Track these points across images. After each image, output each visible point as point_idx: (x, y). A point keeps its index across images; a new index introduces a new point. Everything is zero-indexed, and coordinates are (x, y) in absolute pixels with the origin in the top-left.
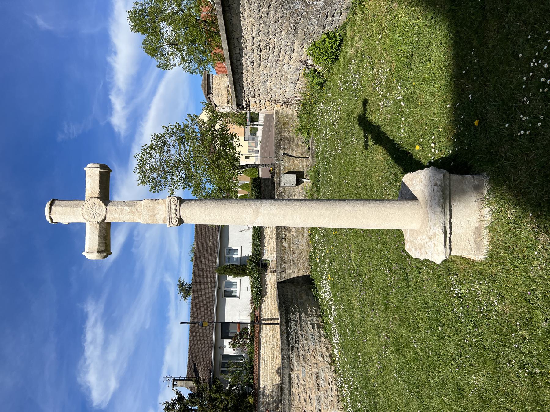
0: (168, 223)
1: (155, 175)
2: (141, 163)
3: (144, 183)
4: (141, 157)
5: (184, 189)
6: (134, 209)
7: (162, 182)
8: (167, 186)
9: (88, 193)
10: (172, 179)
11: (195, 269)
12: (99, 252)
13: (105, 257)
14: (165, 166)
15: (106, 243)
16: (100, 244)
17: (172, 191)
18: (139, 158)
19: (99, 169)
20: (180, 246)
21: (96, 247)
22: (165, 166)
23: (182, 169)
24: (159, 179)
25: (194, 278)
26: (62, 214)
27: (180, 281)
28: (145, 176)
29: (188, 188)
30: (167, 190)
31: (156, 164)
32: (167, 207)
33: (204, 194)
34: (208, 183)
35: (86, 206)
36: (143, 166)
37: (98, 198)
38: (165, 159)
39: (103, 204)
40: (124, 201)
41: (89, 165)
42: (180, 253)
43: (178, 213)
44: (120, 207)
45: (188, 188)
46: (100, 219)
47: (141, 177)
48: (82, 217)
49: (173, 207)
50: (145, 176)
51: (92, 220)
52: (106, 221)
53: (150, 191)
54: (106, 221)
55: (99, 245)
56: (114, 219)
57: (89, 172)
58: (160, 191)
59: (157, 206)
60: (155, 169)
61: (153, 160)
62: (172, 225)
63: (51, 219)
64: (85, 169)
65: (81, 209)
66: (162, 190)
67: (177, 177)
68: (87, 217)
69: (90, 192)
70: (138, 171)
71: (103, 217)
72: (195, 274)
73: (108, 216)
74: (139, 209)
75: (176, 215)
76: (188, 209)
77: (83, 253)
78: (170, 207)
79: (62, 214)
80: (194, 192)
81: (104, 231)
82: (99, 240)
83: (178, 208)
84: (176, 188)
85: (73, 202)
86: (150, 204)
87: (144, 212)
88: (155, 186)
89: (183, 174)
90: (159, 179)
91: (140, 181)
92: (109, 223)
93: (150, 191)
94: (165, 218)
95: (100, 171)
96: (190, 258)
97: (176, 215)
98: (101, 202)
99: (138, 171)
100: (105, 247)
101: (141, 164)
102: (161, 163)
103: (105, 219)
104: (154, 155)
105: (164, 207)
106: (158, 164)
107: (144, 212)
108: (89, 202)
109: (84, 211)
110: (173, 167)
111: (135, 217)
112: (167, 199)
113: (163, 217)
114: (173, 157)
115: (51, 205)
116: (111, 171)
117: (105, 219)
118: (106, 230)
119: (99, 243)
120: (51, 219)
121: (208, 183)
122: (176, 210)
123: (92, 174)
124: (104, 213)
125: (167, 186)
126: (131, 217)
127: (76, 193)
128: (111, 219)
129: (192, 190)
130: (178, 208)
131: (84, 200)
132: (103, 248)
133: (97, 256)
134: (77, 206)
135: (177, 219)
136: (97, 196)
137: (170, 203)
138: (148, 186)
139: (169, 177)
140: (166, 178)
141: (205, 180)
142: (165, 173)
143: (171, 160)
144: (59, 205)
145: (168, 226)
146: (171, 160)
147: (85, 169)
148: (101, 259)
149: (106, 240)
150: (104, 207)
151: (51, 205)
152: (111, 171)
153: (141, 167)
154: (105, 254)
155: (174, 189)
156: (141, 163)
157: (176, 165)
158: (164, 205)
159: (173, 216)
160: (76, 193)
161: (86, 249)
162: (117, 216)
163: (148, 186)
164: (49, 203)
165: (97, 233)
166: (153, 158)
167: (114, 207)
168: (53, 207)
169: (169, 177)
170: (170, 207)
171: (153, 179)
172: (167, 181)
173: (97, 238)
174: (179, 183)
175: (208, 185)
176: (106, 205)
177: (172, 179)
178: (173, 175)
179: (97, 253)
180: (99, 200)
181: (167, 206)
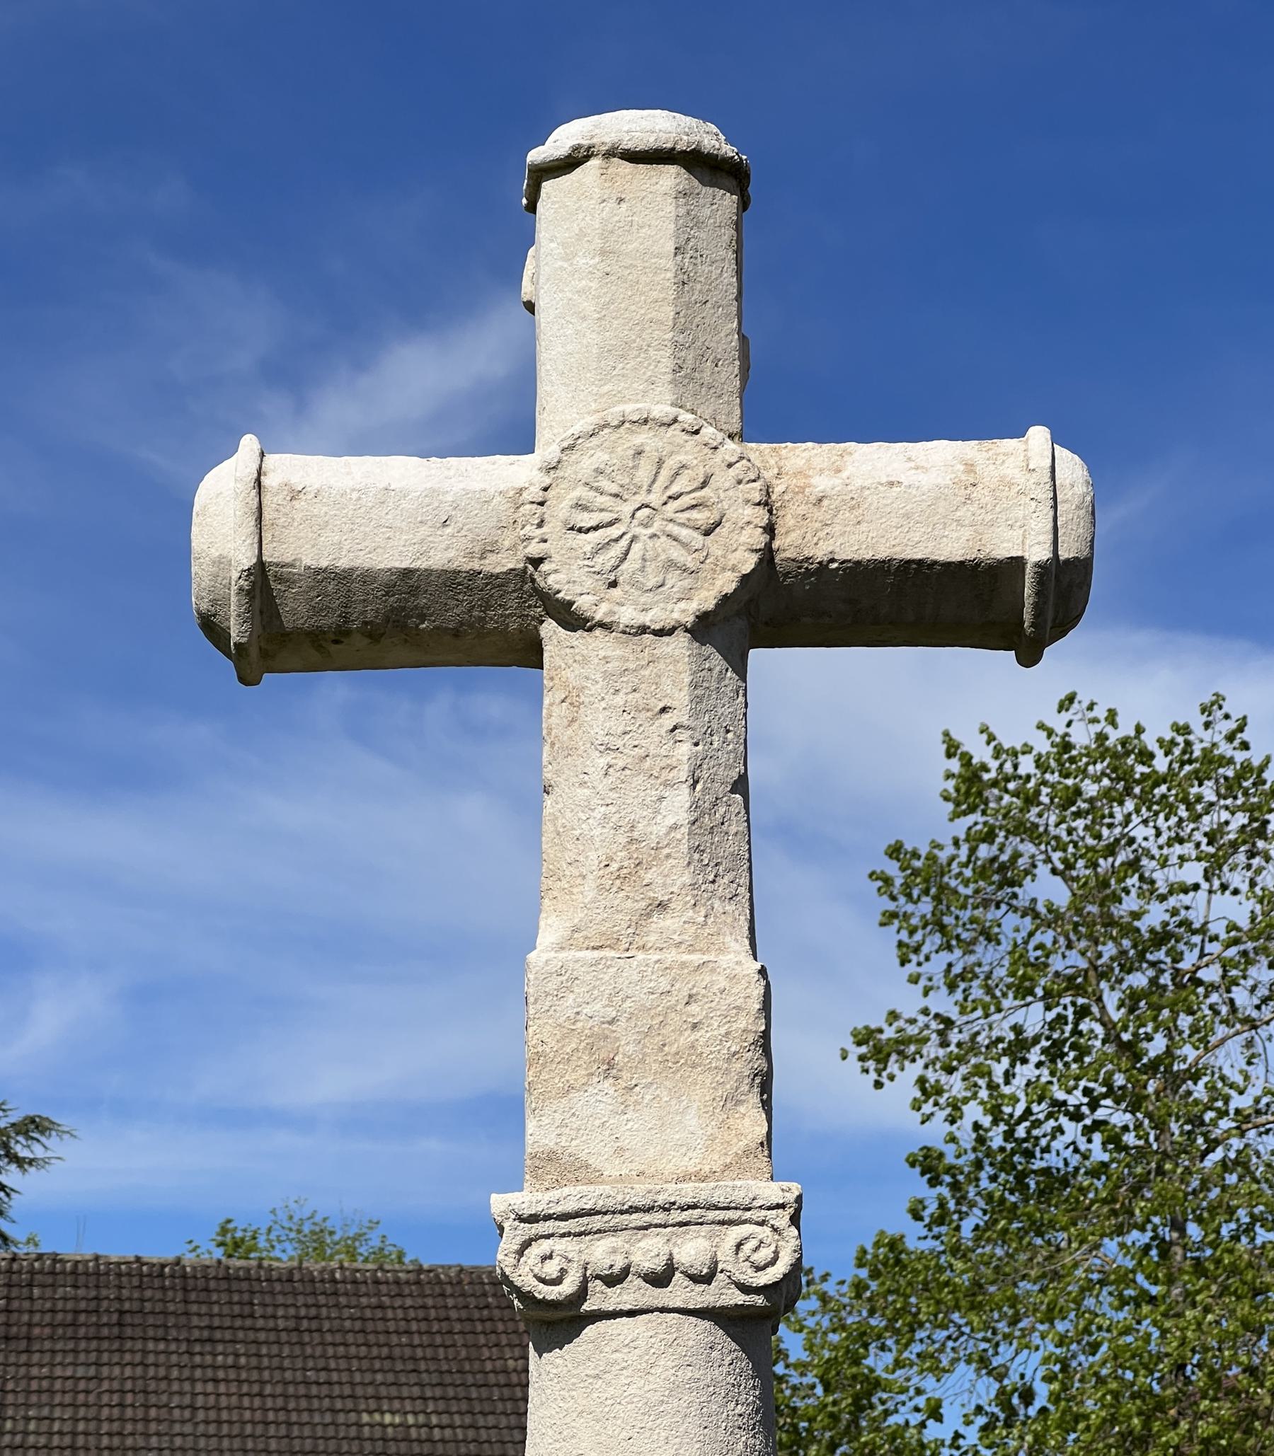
0: (528, 1199)
1: (1048, 889)
2: (1161, 764)
3: (970, 787)
4: (1211, 760)
5: (928, 1164)
6: (673, 876)
7: (986, 954)
8: (944, 1003)
9: (809, 466)
10: (1018, 1048)
11: (145, 1276)
12: (262, 582)
13: (212, 628)
14: (1139, 980)
15: (341, 634)
16: (339, 582)
17: (903, 1048)
18: (1201, 739)
19: (1037, 552)
20: (360, 1120)
21: (306, 547)
22: (1139, 980)
23: (1114, 1140)
24: (1012, 926)
25: (53, 1271)
26: (612, 247)
27: (34, 1126)
28: (1031, 800)
29: (930, 1196)
30: (910, 1002)
31: (1149, 888)
32: (688, 1192)
33: (878, 1362)
34: (987, 1390)
35: (689, 451)
36: (1125, 776)
37: (767, 555)
38: (1211, 974)
39: (706, 599)
40: (740, 785)
41: (1072, 469)
42: (303, 1122)
43: (631, 1294)
44: (685, 749)
45: (930, 1196)
46: (563, 578)
47: (1027, 765)
48: (585, 423)
49: (691, 1250)
50: (1031, 800)
51: (560, 509)
52: (549, 629)
53: (895, 851)
54: (549, 629)
55: (321, 576)
56: (572, 700)
57: (1012, 469)
58: (893, 934)
59: (703, 1088)
60: (1103, 891)
61: (1193, 872)
62: (509, 1243)
63: (569, 164)
64: (1039, 436)
65: (662, 410)
66: (906, 953)
67: (1038, 1092)
68: (586, 462)
69: (821, 483)
70: (1082, 737)
71: (583, 604)
72: (93, 1275)
73: (597, 643)
74: (667, 923)
75: (613, 1280)
76: (674, 1389)
77: (249, 443)
78: (686, 1216)
79: (612, 247)
80: (889, 1258)
81: (455, 614)
82: (368, 577)
83: (680, 1293)
84: (928, 1090)
85: (725, 339)
86: (716, 1029)
87: (638, 975)
88: (943, 895)
89: (1065, 1145)
90: (1012, 926)
91: (981, 753)
92: (531, 654)
93: (895, 851)
94: (579, 1171)
95: (1017, 563)
96: (250, 1212)
97: (613, 1280)
98: (727, 583)
99: (1082, 737)
100: (306, 630)
101: (1146, 757)
102: (1161, 937)
103: (573, 620)
104: (1238, 879)
105: (690, 1163)
106: (1155, 916)
107: (638, 975)
108: (724, 479)
109: (643, 437)
110: (1131, 1050)
111: (589, 890)
112: (773, 1192)
113: (595, 1150)
114: (1229, 1059)
115: (697, 163)
116: (1029, 657)
117: (573, 620)
118: (475, 627)
119: (344, 578)
120: (569, 164)
121: (987, 1390)
122: (660, 1279)
123: (989, 493)
124: (628, 616)
125: (944, 1003)
126: (593, 858)
127: (793, 381)
128: (571, 675)
129: (917, 1239)
130: (680, 1293)
131: (741, 436)
132: (294, 610)
133: (222, 562)
134: (684, 377)
135: (568, 1287)
136: (789, 545)
137: (727, 1214)
138: (936, 827)
139: (1034, 1018)
140: (1023, 990)
141: (1028, 1365)
142: (1072, 983)
143: (1200, 1035)
144: (689, 222)
145: (499, 1203)
146: (1200, 1035)
147: (1039, 436)
148: (199, 599)
149: (373, 633)
150: (686, 612)
151: (697, 163)
152: (1029, 657)
153: (1122, 759)
154: (236, 632)
155: (914, 1070)
156: (1161, 764)
157: (1153, 1083)
158: (715, 1161)
159: (603, 1253)
160: (793, 381)
161: (286, 469)
162: (600, 721)
163: (936, 827)
164: (707, 136)
165: (443, 553)
166: (1214, 867)
167: (680, 698)
168: (670, 177)
169: (1034, 1018)
170: (686, 1216)
171: (1008, 875)
172: (992, 1006)
173: (388, 550)
174: (974, 1112)
175: (963, 1392)
176: (703, 628)
177: (1018, 1048)
178: (1054, 1053)
179: (247, 559)
180: (749, 563)
181: (704, 1192)
